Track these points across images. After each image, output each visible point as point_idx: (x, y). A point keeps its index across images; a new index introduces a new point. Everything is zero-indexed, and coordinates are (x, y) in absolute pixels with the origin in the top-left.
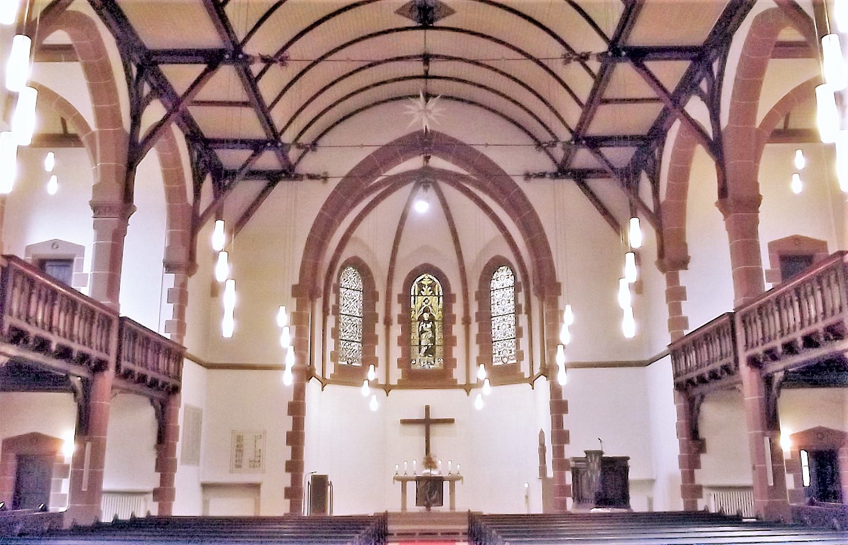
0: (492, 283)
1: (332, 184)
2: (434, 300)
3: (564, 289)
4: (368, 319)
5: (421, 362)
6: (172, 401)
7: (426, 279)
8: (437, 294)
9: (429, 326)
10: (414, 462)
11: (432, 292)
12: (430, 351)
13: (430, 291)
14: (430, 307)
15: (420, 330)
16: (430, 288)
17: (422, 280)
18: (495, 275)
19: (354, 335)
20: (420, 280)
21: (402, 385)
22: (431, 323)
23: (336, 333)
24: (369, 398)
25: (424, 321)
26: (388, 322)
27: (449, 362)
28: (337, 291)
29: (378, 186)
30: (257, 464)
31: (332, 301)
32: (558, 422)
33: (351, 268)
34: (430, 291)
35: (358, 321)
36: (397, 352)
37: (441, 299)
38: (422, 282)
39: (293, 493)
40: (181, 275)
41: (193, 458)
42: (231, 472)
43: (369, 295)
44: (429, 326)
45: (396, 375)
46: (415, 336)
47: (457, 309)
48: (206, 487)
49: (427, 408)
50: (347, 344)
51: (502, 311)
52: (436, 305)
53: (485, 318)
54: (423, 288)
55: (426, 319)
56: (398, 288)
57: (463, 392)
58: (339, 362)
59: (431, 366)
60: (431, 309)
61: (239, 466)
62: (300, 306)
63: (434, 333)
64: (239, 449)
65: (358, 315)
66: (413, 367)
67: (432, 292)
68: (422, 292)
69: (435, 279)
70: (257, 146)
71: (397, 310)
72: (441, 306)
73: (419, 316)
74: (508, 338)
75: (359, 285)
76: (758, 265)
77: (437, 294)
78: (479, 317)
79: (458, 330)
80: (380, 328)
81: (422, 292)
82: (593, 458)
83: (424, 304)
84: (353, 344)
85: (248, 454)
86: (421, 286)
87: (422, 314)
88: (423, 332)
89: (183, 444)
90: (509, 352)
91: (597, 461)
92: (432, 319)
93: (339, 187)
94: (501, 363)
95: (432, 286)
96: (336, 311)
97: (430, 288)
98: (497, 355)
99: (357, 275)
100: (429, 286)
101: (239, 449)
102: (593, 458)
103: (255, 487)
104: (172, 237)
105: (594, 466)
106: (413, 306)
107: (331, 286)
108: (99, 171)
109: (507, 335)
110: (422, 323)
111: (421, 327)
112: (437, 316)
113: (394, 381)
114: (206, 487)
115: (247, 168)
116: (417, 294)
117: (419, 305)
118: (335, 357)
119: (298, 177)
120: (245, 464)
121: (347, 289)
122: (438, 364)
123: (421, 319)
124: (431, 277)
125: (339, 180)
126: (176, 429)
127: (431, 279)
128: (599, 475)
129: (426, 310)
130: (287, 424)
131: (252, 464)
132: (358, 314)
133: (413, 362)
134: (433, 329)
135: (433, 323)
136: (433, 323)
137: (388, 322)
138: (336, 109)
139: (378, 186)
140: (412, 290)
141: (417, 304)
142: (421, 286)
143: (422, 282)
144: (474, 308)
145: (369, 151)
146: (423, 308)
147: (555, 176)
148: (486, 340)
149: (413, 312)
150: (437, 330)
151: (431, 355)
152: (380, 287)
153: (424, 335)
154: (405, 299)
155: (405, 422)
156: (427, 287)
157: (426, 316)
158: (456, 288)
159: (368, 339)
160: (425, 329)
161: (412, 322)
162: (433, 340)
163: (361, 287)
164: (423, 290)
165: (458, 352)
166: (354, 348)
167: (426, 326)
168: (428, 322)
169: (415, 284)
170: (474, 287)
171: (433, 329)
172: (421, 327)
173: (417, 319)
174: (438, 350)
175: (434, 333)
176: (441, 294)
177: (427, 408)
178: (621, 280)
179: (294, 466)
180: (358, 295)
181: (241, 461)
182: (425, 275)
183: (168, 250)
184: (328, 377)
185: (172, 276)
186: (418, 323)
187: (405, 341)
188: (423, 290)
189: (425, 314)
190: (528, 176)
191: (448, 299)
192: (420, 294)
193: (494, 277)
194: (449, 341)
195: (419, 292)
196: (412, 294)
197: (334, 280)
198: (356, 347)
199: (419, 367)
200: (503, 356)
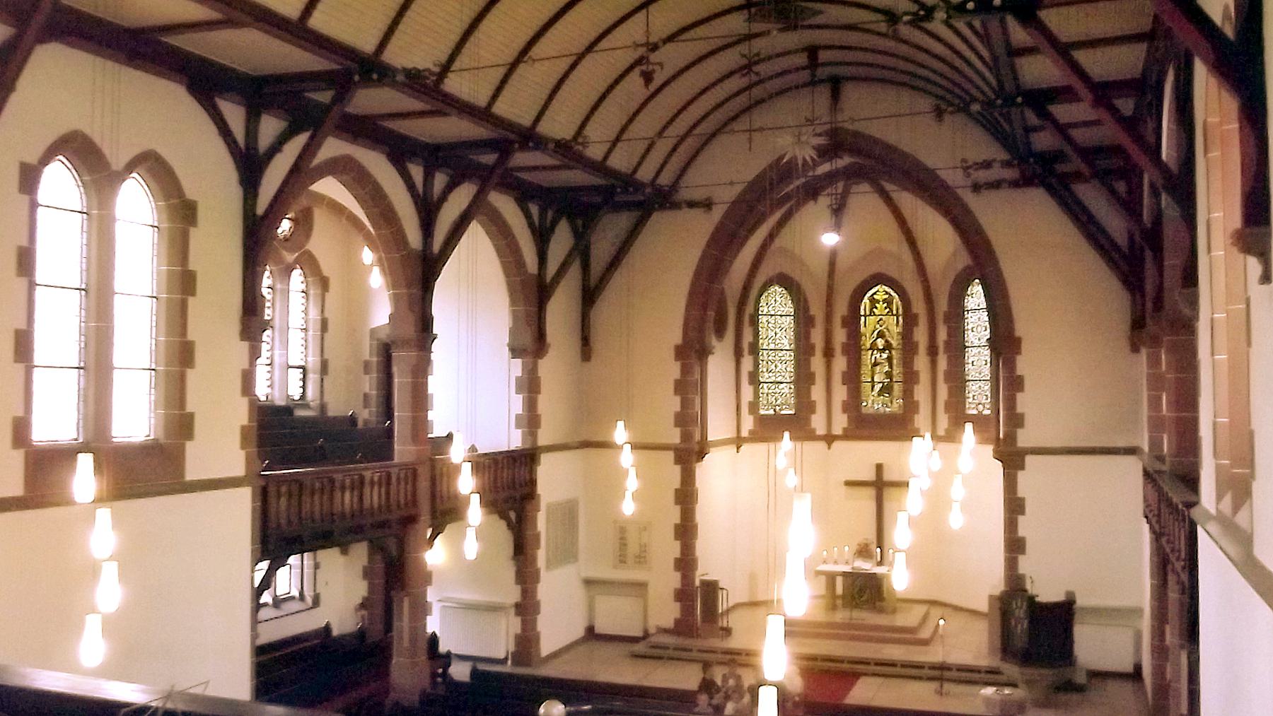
0: (966, 301)
1: (717, 213)
2: (891, 321)
3: (1025, 346)
4: (803, 350)
5: (873, 402)
6: (529, 507)
7: (880, 291)
8: (895, 312)
9: (885, 356)
10: (847, 548)
11: (888, 310)
12: (886, 390)
13: (886, 308)
14: (885, 330)
15: (873, 361)
16: (885, 305)
17: (875, 294)
18: (969, 289)
19: (783, 374)
20: (872, 295)
21: (847, 436)
22: (887, 352)
23: (754, 379)
24: (785, 471)
25: (878, 349)
26: (828, 353)
27: (910, 407)
28: (754, 322)
29: (788, 197)
30: (642, 560)
31: (747, 338)
32: (1011, 525)
33: (777, 288)
34: (886, 308)
35: (789, 356)
36: (840, 393)
37: (900, 319)
38: (875, 296)
39: (684, 595)
40: (529, 360)
41: (566, 553)
42: (615, 567)
43: (803, 320)
44: (885, 356)
45: (841, 422)
46: (866, 370)
47: (921, 335)
48: (589, 583)
49: (879, 467)
50: (773, 387)
51: (977, 341)
52: (894, 327)
53: (957, 348)
54: (877, 305)
55: (881, 347)
56: (841, 309)
57: (822, 445)
58: (762, 412)
59: (888, 409)
60: (887, 333)
61: (623, 562)
62: (686, 370)
63: (891, 366)
64: (623, 543)
65: (788, 348)
66: (864, 411)
67: (888, 310)
68: (874, 310)
69: (892, 293)
70: (503, 147)
71: (840, 336)
72: (899, 329)
73: (871, 342)
74: (984, 378)
75: (789, 308)
76: (1194, 412)
77: (895, 312)
78: (948, 344)
79: (921, 362)
80: (817, 363)
81: (874, 310)
82: (1019, 604)
83: (878, 326)
84: (781, 386)
85: (633, 549)
86: (873, 301)
87: (876, 339)
88: (875, 364)
89: (547, 553)
90: (985, 397)
91: (1024, 607)
92: (888, 346)
93: (727, 215)
94: (975, 412)
95: (888, 302)
96: (755, 349)
97: (885, 305)
98: (970, 400)
99: (785, 295)
100: (884, 301)
101: (623, 543)
102: (1019, 604)
103: (639, 588)
104: (515, 316)
105: (1019, 612)
106: (863, 329)
107: (748, 317)
108: (392, 297)
109: (983, 374)
110: (875, 352)
111: (873, 358)
112: (894, 343)
113: (838, 430)
114: (589, 583)
115: (389, 469)
116: (868, 313)
117: (870, 328)
118: (754, 407)
119: (676, 206)
120: (630, 560)
121: (772, 315)
122: (896, 406)
123: (873, 347)
124: (887, 289)
125: (725, 207)
126: (537, 536)
127: (887, 293)
128: (1025, 626)
129: (881, 335)
130: (675, 549)
131: (638, 560)
132: (788, 345)
133: (864, 404)
134: (889, 359)
135: (890, 352)
136: (890, 352)
137: (828, 353)
138: (681, 149)
139: (788, 197)
140: (862, 308)
141: (868, 326)
142: (873, 301)
143: (875, 296)
144: (942, 335)
145: (738, 189)
146: (878, 330)
147: (1015, 184)
148: (958, 380)
149: (863, 338)
150: (895, 362)
151: (887, 395)
152: (817, 310)
153: (878, 368)
154: (852, 321)
155: (849, 484)
156: (881, 303)
157: (880, 343)
158: (919, 307)
159: (803, 379)
160: (879, 360)
161: (862, 350)
162: (889, 375)
163: (792, 310)
164: (876, 308)
165: (921, 393)
166: (783, 391)
167: (881, 356)
168: (883, 350)
169: (866, 300)
170: (942, 305)
171: (889, 359)
172: (873, 358)
173: (868, 346)
174: (897, 388)
175: (891, 366)
176: (901, 311)
177: (879, 467)
178: (770, 616)
179: (686, 563)
180: (788, 322)
181: (625, 556)
182: (879, 286)
183: (513, 332)
184: (745, 433)
185: (519, 362)
186: (870, 352)
187: (853, 379)
188: (876, 308)
189: (879, 340)
190: (976, 188)
191: (909, 321)
192: (872, 313)
193: (969, 292)
194: (910, 378)
195: (871, 310)
196: (862, 313)
197: (749, 309)
198: (786, 389)
199: (871, 411)
200: (977, 401)
